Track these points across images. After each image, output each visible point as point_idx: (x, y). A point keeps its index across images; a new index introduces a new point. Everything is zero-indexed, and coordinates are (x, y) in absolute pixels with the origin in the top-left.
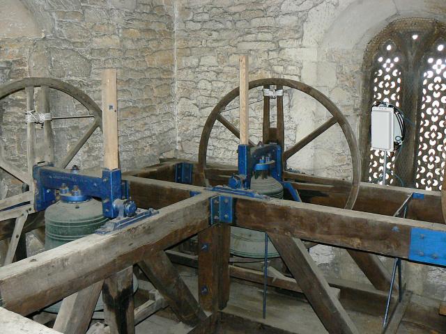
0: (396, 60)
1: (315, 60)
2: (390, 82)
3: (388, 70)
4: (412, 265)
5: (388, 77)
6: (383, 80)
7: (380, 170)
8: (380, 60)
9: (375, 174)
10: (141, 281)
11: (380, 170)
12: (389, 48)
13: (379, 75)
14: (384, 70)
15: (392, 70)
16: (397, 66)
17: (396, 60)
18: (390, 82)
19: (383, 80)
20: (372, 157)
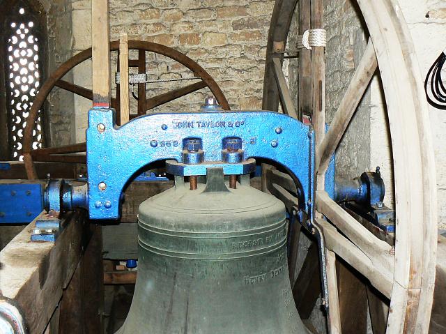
0: (31, 24)
1: (45, 211)
2: (27, 76)
3: (23, 36)
4: (80, 11)
5: (25, 98)
6: (20, 101)
7: (23, 100)
8: (13, 25)
9: (19, 104)
10: (91, 89)
11: (23, 100)
12: (22, 11)
13: (16, 96)
14: (18, 37)
15: (27, 36)
16: (32, 32)
17: (31, 24)
18: (27, 76)
19: (20, 101)
20: (13, 112)
